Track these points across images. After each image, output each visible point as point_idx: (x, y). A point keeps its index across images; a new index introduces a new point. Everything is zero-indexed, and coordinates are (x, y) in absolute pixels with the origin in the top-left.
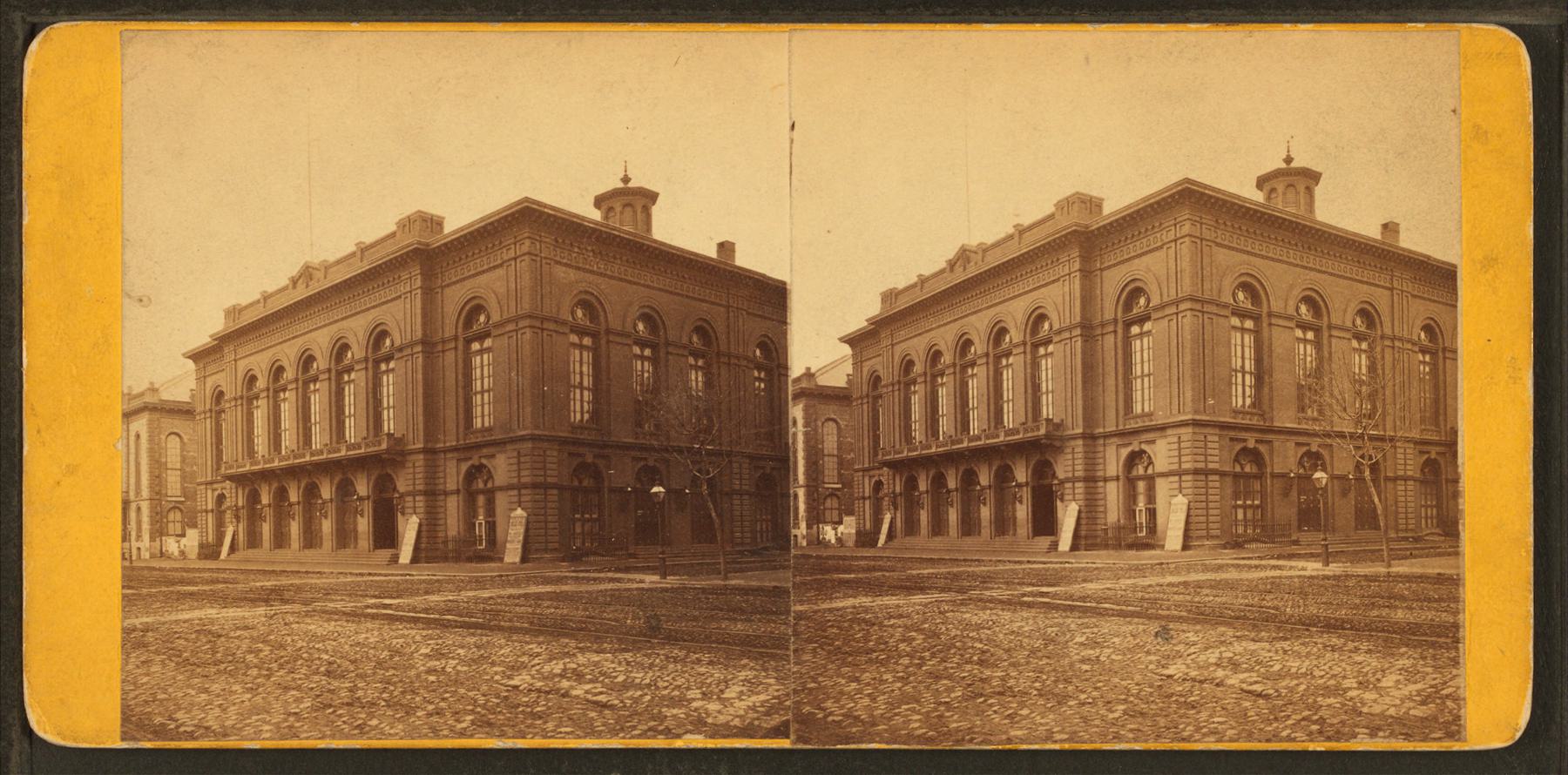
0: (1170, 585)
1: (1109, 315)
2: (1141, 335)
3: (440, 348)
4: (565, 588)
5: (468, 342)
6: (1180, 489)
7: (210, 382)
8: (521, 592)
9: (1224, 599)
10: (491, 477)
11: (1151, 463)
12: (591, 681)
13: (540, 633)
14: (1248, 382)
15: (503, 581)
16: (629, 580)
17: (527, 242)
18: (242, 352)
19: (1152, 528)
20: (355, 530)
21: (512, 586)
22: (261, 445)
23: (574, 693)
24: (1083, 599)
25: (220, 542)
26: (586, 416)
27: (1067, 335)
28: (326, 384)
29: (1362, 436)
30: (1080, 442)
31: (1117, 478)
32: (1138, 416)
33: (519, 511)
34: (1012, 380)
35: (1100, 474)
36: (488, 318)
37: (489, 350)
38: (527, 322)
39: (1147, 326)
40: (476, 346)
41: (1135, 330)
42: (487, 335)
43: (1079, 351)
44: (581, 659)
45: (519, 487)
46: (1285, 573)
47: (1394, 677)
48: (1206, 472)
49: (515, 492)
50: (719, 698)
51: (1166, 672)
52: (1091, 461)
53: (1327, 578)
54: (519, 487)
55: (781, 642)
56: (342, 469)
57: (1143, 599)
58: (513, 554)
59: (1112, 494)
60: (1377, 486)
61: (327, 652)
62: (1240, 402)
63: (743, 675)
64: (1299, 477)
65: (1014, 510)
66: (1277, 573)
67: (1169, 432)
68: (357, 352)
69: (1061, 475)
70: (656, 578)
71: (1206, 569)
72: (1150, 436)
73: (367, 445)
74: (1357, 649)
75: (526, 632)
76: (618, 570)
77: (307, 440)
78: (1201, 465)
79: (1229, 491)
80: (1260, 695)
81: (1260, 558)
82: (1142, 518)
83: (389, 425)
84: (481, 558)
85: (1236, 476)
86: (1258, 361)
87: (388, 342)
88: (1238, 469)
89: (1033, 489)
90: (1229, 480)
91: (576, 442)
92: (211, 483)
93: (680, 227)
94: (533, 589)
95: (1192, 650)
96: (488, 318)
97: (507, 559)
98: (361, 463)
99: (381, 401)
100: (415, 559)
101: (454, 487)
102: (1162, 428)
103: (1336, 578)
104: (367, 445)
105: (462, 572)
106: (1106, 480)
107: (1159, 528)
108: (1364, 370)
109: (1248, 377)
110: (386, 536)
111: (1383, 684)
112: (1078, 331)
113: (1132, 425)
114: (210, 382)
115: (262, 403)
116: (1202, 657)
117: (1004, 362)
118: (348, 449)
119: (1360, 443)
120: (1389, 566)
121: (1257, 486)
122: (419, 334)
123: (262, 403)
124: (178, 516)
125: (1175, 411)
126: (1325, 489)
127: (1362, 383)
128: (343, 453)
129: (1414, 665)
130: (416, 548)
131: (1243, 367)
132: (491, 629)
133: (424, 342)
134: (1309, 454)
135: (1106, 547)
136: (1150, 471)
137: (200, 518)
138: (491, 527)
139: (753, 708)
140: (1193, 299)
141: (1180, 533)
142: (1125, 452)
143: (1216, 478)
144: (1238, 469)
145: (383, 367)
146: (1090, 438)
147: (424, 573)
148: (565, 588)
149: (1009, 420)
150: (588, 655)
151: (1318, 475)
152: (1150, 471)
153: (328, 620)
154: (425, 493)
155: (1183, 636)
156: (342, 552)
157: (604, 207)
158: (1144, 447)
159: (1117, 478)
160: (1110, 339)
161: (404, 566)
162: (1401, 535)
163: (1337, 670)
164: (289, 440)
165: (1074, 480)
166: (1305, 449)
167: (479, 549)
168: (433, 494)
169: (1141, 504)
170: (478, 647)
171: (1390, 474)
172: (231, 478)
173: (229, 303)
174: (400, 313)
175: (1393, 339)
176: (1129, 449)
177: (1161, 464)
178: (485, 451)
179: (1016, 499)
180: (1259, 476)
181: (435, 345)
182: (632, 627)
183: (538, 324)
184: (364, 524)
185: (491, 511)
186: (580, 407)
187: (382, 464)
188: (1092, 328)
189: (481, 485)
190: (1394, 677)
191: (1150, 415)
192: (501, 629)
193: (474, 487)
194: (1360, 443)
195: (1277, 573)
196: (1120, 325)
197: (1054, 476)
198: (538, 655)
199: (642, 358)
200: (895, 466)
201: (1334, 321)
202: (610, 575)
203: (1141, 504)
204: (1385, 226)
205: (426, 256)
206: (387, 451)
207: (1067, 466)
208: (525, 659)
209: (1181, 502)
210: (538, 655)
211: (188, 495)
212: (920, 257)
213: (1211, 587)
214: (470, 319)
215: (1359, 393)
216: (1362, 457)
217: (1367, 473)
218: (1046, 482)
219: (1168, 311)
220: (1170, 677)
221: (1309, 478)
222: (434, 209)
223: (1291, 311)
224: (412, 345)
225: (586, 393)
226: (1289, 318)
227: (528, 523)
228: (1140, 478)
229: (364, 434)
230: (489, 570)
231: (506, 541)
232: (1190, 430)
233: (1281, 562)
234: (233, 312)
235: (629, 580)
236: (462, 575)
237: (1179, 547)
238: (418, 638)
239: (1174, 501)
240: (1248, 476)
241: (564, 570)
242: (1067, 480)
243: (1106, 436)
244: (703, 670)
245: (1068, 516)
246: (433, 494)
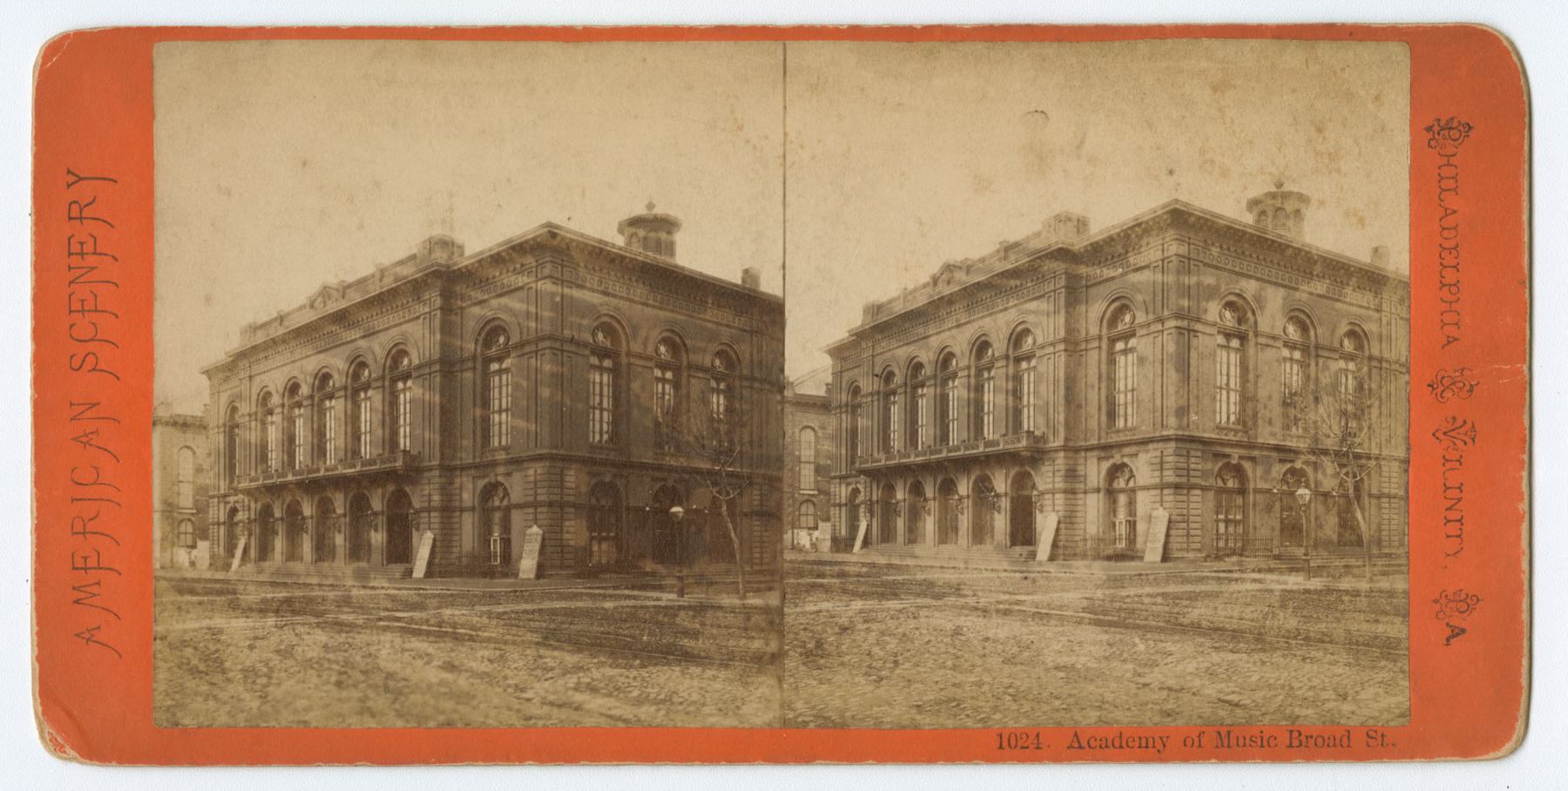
0: (525, 612)
1: (1094, 331)
2: (500, 372)
3: (1083, 346)
4: (580, 604)
5: (1112, 341)
6: (536, 521)
7: (847, 376)
8: (535, 607)
9: (580, 627)
10: (506, 494)
11: (1132, 476)
12: (1223, 681)
13: (1173, 632)
14: (1232, 399)
15: (517, 595)
16: (647, 598)
17: (549, 266)
18: (256, 369)
19: (1132, 540)
20: (993, 528)
21: (526, 602)
22: (897, 441)
23: (1207, 691)
24: (1061, 607)
25: (853, 539)
26: (605, 437)
27: (427, 370)
28: (342, 400)
29: (1346, 455)
30: (1062, 454)
31: (473, 509)
32: (1118, 431)
33: (535, 529)
34: (994, 399)
35: (457, 504)
36: (508, 339)
37: (507, 371)
38: (548, 344)
39: (1132, 342)
40: (495, 366)
41: (1120, 346)
42: (1133, 335)
43: (1062, 365)
44: (596, 674)
45: (535, 505)
46: (639, 603)
47: (1372, 691)
48: (562, 505)
49: (531, 510)
50: (1354, 700)
51: (1142, 680)
52: (446, 491)
53: (1307, 591)
54: (535, 505)
55: (777, 657)
56: (357, 486)
57: (1120, 609)
58: (527, 565)
59: (468, 526)
60: (733, 522)
61: (337, 663)
62: (597, 438)
63: (1379, 677)
64: (1283, 493)
65: (992, 520)
66: (631, 603)
67: (1151, 446)
68: (999, 346)
69: (1041, 486)
70: (673, 596)
71: (562, 597)
72: (1133, 449)
73: (383, 462)
74: (715, 678)
75: (1161, 630)
76: (633, 588)
77: (944, 437)
78: (1184, 480)
79: (1211, 505)
80: (1237, 705)
81: (615, 588)
82: (1122, 530)
83: (404, 442)
84: (490, 573)
85: (1220, 491)
86: (616, 399)
87: (406, 361)
88: (1220, 484)
89: (1012, 499)
90: (1211, 495)
91: (593, 462)
92: (225, 496)
93: (703, 252)
94: (546, 605)
95: (1170, 659)
96: (508, 339)
97: (521, 575)
98: (376, 479)
99: (397, 418)
100: (429, 573)
101: (470, 504)
102: (1144, 442)
103: (1319, 592)
104: (383, 462)
105: (477, 586)
106: (462, 510)
107: (514, 556)
108: (722, 409)
109: (1232, 394)
110: (400, 553)
111: (1363, 696)
112: (437, 367)
113: (1114, 438)
114: (847, 376)
115: (277, 418)
116: (1180, 668)
117: (986, 375)
118: (363, 465)
119: (1344, 461)
120: (744, 597)
121: (1239, 501)
122: (1062, 334)
123: (277, 418)
124: (811, 510)
125: (532, 445)
126: (1308, 506)
127: (720, 421)
128: (981, 449)
129: (1393, 679)
130: (430, 564)
131: (601, 402)
132: (1126, 627)
133: (1065, 340)
134: (1293, 471)
135: (460, 574)
136: (1131, 484)
137: (213, 530)
138: (507, 543)
139: (1388, 710)
140: (550, 338)
141: (1048, 548)
142: (1106, 465)
143: (1198, 492)
144: (1220, 484)
145: (400, 385)
146: (1071, 449)
147: (436, 587)
148: (580, 604)
149: (366, 450)
150: (1222, 655)
151: (1300, 491)
152: (1131, 484)
153: (339, 632)
154: (1065, 492)
155: (1161, 645)
156: (943, 547)
157: (1257, 210)
158: (1126, 460)
159: (473, 509)
160: (1094, 355)
161: (419, 580)
162: (757, 568)
163: (1316, 682)
164: (926, 434)
165: (429, 510)
166: (1288, 465)
167: (492, 564)
168: (448, 509)
169: (1122, 516)
170: (491, 661)
171: (1374, 491)
172: (862, 472)
173: (244, 323)
174: (418, 334)
175: (1381, 360)
176: (1111, 462)
177: (517, 495)
178: (1126, 450)
179: (994, 507)
180: (1242, 491)
181: (452, 365)
182: (649, 643)
183: (557, 345)
184: (378, 538)
185: (1131, 503)
186: (599, 427)
187: (399, 477)
188: (1077, 344)
189: (497, 503)
190: (1372, 691)
191: (1134, 429)
192: (1138, 627)
193: (1115, 485)
194: (1344, 461)
195: (631, 603)
196: (1105, 340)
197: (1034, 487)
198: (552, 669)
199: (663, 380)
200: (874, 475)
201: (1321, 342)
202: (627, 592)
203: (1122, 516)
204: (1376, 250)
205: (444, 281)
206: (1026, 449)
207: (425, 494)
208: (1157, 657)
209: (1162, 516)
210: (552, 669)
211: (201, 509)
212: (897, 279)
213: (1190, 599)
214: (489, 341)
215: (717, 431)
216: (1347, 474)
217: (724, 508)
218: (1025, 493)
219: (527, 349)
220: (529, 700)
221: (1292, 494)
222: (1077, 209)
223: (650, 350)
224: (430, 363)
225: (605, 414)
226: (649, 359)
227: (544, 539)
228: (1122, 491)
229: (1003, 431)
230: (500, 585)
231: (521, 558)
232: (1173, 444)
233: (635, 593)
234: (875, 309)
235: (647, 598)
236: (477, 590)
237: (1158, 558)
238: (1048, 635)
239: (1155, 513)
240: (1229, 491)
241: (579, 587)
242: (422, 510)
243: (463, 468)
244: (1340, 671)
245: (1046, 524)
246: (448, 509)
